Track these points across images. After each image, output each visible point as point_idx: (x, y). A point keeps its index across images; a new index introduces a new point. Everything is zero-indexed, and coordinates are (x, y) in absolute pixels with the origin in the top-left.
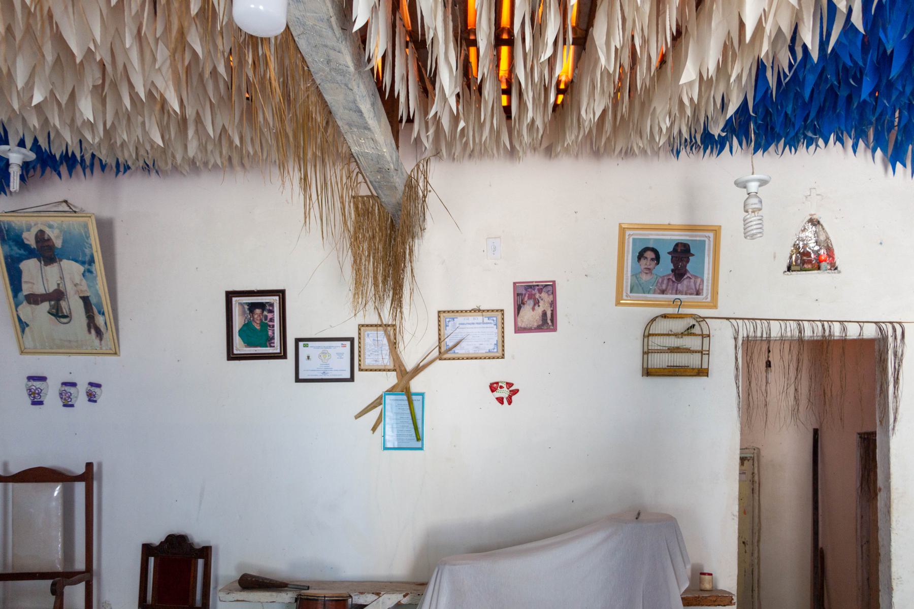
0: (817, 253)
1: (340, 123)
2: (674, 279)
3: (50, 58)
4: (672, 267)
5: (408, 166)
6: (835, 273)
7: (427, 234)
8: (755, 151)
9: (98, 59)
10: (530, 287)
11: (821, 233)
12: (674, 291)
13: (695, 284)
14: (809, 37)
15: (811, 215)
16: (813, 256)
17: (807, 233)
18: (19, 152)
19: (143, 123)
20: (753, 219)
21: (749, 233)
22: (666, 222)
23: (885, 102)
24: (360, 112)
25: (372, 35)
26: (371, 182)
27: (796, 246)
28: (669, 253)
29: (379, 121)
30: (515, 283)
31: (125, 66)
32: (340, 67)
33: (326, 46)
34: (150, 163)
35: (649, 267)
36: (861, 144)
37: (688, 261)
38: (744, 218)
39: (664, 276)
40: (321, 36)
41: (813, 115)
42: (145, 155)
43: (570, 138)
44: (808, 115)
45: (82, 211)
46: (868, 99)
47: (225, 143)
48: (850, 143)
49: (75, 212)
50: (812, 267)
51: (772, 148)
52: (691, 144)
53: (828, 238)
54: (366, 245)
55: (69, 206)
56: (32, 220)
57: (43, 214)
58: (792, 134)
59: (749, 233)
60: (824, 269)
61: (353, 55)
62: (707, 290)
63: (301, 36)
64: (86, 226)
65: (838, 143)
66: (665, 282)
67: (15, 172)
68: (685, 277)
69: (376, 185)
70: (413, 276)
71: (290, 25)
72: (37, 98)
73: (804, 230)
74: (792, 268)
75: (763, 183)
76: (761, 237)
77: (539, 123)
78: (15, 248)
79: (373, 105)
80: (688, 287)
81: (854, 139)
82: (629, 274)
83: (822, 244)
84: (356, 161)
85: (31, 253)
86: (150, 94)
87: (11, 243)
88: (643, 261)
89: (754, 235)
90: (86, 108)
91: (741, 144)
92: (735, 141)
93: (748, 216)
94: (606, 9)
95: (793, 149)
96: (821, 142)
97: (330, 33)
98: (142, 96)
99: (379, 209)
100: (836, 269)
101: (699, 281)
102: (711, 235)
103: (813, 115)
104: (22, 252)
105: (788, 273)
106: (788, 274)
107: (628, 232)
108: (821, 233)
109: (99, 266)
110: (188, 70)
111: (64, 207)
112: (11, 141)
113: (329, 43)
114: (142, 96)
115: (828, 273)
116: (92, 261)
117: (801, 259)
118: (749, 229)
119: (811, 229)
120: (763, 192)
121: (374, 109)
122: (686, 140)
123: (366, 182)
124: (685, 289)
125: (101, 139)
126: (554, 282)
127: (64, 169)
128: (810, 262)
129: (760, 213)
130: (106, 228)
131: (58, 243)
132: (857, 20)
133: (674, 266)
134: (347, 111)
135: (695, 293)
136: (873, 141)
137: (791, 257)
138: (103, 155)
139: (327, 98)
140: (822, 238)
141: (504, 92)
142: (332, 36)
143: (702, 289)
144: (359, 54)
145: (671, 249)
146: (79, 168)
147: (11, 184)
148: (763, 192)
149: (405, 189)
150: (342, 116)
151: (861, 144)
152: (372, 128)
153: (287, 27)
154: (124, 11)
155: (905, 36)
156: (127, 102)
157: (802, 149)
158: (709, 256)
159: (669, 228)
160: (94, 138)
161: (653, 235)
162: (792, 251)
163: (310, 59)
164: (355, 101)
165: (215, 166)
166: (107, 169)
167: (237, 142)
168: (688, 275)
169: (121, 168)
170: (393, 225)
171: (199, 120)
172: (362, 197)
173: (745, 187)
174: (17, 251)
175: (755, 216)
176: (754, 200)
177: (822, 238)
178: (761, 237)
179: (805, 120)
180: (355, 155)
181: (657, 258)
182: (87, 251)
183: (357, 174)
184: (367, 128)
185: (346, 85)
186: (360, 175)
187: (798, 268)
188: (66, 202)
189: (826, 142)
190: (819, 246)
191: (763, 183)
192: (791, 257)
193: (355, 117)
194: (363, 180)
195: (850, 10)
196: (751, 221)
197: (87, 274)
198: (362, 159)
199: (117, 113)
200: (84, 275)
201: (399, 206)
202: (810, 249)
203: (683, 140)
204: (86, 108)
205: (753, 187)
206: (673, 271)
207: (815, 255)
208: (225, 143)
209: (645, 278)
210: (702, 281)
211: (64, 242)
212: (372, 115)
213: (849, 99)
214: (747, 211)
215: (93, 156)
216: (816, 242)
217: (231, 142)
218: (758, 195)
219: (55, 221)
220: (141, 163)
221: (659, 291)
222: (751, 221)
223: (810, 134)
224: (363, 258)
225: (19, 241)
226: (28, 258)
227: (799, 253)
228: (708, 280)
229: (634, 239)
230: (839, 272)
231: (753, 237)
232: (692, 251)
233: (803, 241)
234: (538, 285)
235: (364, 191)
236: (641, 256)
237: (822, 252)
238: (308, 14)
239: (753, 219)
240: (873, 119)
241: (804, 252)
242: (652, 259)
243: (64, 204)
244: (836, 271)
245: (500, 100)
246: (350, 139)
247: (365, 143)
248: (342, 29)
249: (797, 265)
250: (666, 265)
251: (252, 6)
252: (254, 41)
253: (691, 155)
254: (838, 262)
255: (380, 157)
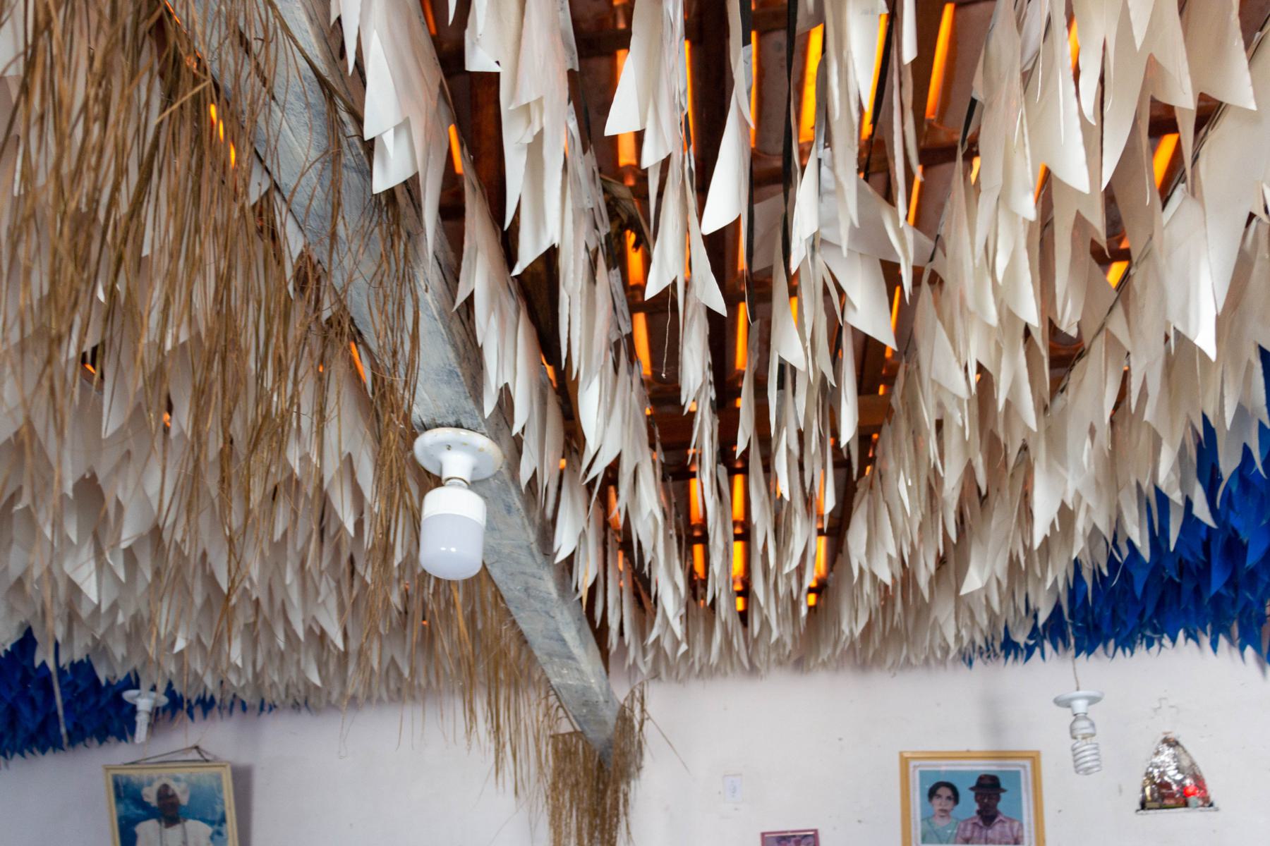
0: (1179, 783)
1: (537, 653)
2: (981, 823)
3: (198, 600)
4: (976, 807)
5: (621, 693)
6: (1210, 811)
7: (644, 774)
8: (1077, 654)
9: (254, 598)
10: (784, 838)
11: (1183, 756)
12: (983, 840)
13: (1011, 829)
14: (1137, 534)
15: (1165, 733)
16: (1175, 787)
17: (1162, 758)
18: (149, 697)
19: (298, 662)
20: (1081, 745)
21: (1081, 767)
22: (964, 748)
23: (1248, 595)
24: (563, 641)
25: (580, 563)
26: (574, 716)
27: (1149, 776)
28: (972, 789)
29: (586, 648)
30: (763, 834)
31: (283, 604)
32: (541, 594)
33: (523, 573)
34: (301, 701)
35: (945, 808)
36: (1223, 641)
37: (998, 799)
38: (1072, 747)
39: (967, 820)
40: (518, 563)
41: (1149, 612)
42: (297, 694)
43: (825, 653)
44: (1144, 610)
45: (216, 759)
46: (1223, 591)
47: (393, 674)
48: (1206, 641)
49: (207, 761)
50: (1177, 803)
51: (1100, 649)
52: (987, 652)
53: (1193, 764)
54: (567, 795)
55: (200, 753)
56: (155, 773)
57: (168, 765)
58: (1124, 634)
59: (1081, 767)
60: (1194, 805)
61: (557, 585)
62: (1030, 837)
63: (496, 565)
64: (219, 777)
65: (1190, 641)
66: (969, 827)
67: (142, 720)
68: (997, 820)
69: (581, 719)
70: (629, 833)
71: (487, 562)
72: (180, 645)
73: (1158, 753)
74: (1148, 805)
75: (1093, 700)
76: (1098, 771)
77: (788, 640)
78: (132, 808)
79: (579, 631)
80: (1002, 834)
81: (1212, 635)
82: (918, 818)
83: (1187, 772)
84: (556, 694)
85: (150, 813)
86: (309, 631)
87: (128, 801)
88: (936, 801)
89: (1089, 768)
90: (236, 652)
91: (1056, 648)
92: (1048, 646)
93: (1078, 745)
94: (865, 514)
95: (1128, 651)
96: (1166, 641)
97: (530, 560)
98: (301, 634)
99: (583, 748)
100: (1211, 805)
101: (1016, 825)
102: (1028, 763)
103: (1149, 612)
104: (140, 812)
105: (1142, 812)
106: (1142, 814)
107: (913, 763)
108: (1183, 756)
109: (231, 827)
110: (355, 604)
111: (194, 755)
112: (142, 684)
113: (528, 570)
114: (301, 634)
115: (1201, 811)
116: (223, 820)
117: (1159, 793)
118: (1081, 761)
119: (1168, 752)
120: (1096, 712)
121: (580, 636)
122: (980, 648)
123: (568, 717)
124: (998, 837)
125: (247, 681)
126: (816, 831)
127: (198, 712)
128: (1172, 796)
129: (1094, 740)
130: (243, 779)
131: (184, 800)
132: (1202, 511)
133: (980, 806)
134: (547, 641)
135: (1012, 841)
136: (1239, 637)
137: (1143, 791)
138: (248, 697)
139: (524, 627)
140: (1185, 763)
141: (739, 594)
142: (531, 563)
143: (1022, 837)
144: (563, 577)
145: (973, 783)
146: (215, 709)
147: (137, 735)
148: (1096, 712)
149: (617, 723)
150: (540, 645)
151: (1223, 641)
152: (577, 657)
153: (484, 564)
154: (286, 549)
155: (1264, 522)
156: (281, 641)
157: (1141, 651)
158: (1027, 791)
159: (968, 755)
160: (239, 681)
161: (945, 766)
162: (1144, 782)
163: (505, 588)
164: (557, 630)
165: (380, 700)
166: (248, 711)
167: (406, 673)
168: (1000, 817)
169: (264, 707)
170: (601, 765)
171: (361, 653)
172: (563, 735)
173: (1069, 706)
174: (135, 811)
175: (1087, 744)
176: (1082, 724)
177: (1185, 763)
178: (1098, 771)
179: (1141, 616)
180: (555, 687)
181: (955, 797)
182: (218, 808)
183: (557, 709)
184: (571, 657)
185: (547, 613)
186: (561, 711)
187: (1156, 805)
188: (197, 748)
189: (1174, 640)
190: (1183, 773)
191: (1093, 700)
192: (1143, 791)
193: (557, 647)
194: (565, 715)
195: (1189, 504)
196: (1084, 751)
197: (216, 837)
198: (563, 692)
199: (269, 652)
200: (212, 838)
201: (610, 743)
202: (1169, 777)
203: (977, 648)
204: (236, 652)
205: (1080, 706)
206: (979, 812)
207: (1178, 786)
208: (393, 674)
209: (940, 823)
210: (1021, 825)
211: (192, 797)
212: (578, 642)
213: (1198, 592)
214: (1075, 738)
215: (235, 696)
216: (1177, 768)
217: (400, 674)
218: (1088, 716)
219: (182, 773)
220: (290, 701)
221: (961, 841)
222: (1084, 751)
223: (1148, 633)
224: (564, 813)
225: (138, 801)
226: (146, 819)
227: (1155, 783)
228: (1029, 824)
229: (921, 772)
230: (1217, 810)
231: (1087, 771)
232: (1003, 785)
233: (1158, 767)
234: (794, 836)
235: (565, 727)
236: (932, 793)
237: (1188, 782)
238: (505, 542)
239: (1086, 748)
240: (1236, 615)
241: (1161, 782)
242: (949, 798)
243: (195, 751)
244: (1211, 808)
245: (735, 605)
246: (550, 672)
247: (568, 674)
248: (545, 554)
249: (1153, 800)
250: (969, 805)
251: (443, 549)
252: (442, 586)
253: (989, 661)
254: (1213, 798)
255: (587, 689)
